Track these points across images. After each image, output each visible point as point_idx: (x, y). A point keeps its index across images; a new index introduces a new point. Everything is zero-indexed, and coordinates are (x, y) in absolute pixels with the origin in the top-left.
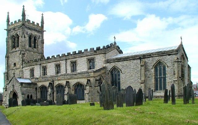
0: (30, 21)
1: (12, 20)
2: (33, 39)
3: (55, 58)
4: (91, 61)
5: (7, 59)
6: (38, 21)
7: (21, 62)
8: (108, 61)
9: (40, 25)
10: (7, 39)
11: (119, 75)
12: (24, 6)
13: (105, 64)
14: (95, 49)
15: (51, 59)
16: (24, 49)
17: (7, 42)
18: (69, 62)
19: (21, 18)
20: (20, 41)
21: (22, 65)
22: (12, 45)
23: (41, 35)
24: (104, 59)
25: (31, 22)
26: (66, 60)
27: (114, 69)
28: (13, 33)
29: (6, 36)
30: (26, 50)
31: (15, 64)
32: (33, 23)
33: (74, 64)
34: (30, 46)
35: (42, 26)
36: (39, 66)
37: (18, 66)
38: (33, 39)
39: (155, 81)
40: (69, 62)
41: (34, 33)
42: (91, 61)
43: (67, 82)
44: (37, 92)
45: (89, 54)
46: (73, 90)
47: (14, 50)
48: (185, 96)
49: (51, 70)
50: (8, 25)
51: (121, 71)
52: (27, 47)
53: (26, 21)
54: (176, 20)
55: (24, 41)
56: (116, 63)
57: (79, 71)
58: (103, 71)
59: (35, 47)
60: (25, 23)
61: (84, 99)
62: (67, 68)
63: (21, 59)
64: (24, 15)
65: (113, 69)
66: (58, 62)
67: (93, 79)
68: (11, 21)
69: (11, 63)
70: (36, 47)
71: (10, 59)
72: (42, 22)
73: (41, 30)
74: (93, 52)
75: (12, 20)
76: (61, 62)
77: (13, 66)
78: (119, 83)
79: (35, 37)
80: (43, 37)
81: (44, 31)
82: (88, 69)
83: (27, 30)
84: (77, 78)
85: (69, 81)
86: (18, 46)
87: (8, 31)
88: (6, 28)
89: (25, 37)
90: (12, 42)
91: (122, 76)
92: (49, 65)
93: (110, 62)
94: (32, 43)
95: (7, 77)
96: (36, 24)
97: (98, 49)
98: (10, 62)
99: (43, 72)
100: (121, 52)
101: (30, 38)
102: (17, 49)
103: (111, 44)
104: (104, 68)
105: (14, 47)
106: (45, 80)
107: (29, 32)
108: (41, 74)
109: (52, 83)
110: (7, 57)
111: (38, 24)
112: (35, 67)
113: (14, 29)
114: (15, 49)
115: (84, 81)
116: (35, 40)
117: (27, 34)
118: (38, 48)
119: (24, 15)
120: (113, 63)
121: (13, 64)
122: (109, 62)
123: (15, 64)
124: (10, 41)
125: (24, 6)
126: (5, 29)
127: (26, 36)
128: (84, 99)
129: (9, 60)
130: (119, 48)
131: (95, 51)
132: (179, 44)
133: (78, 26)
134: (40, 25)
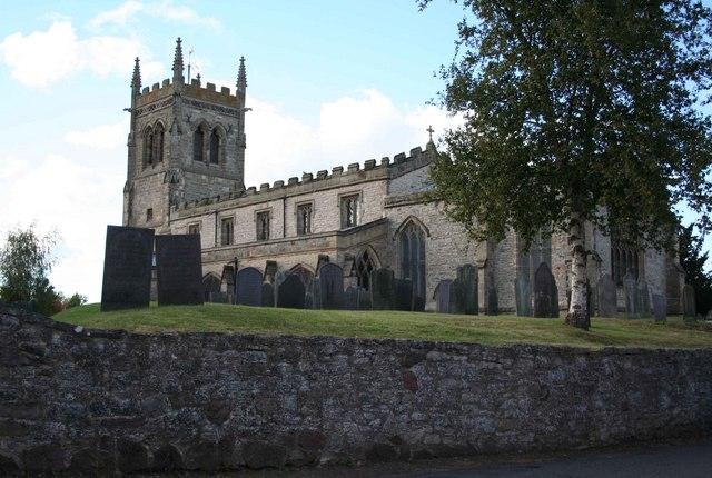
1: (147, 81)
2: (207, 136)
3: (256, 193)
4: (348, 203)
5: (127, 195)
6: (225, 80)
7: (166, 205)
8: (392, 204)
9: (233, 93)
10: (132, 138)
14: (362, 167)
15: (331, 177)
16: (177, 166)
17: (132, 145)
18: (292, 202)
19: (170, 75)
20: (166, 143)
21: (169, 214)
22: (145, 155)
23: (233, 121)
24: (384, 196)
26: (285, 198)
27: (409, 224)
28: (149, 119)
29: (127, 129)
30: (185, 170)
31: (150, 212)
33: (305, 211)
34: (199, 156)
35: (241, 94)
36: (213, 216)
38: (207, 136)
39: (519, 262)
41: (212, 117)
42: (348, 203)
43: (270, 264)
45: (344, 180)
47: (150, 169)
48: (611, 441)
49: (245, 231)
50: (136, 94)
51: (428, 231)
52: (189, 160)
55: (178, 145)
56: (416, 207)
58: (375, 233)
59: (215, 159)
60: (185, 92)
62: (288, 221)
63: (167, 197)
66: (264, 206)
67: (338, 256)
68: (144, 84)
69: (139, 209)
70: (220, 160)
71: (138, 197)
73: (232, 105)
74: (356, 176)
75: (147, 81)
76: (271, 204)
77: (144, 217)
79: (215, 131)
80: (241, 126)
81: (246, 110)
83: (186, 110)
84: (297, 253)
86: (161, 160)
87: (135, 113)
89: (180, 132)
90: (145, 146)
91: (430, 245)
92: (239, 213)
96: (218, 90)
97: (371, 165)
98: (136, 207)
99: (225, 234)
101: (199, 132)
102: (159, 167)
103: (416, 151)
104: (382, 222)
105: (150, 160)
106: (216, 257)
107: (197, 115)
108: (219, 241)
110: (130, 190)
111: (226, 90)
112: (204, 219)
114: (153, 167)
118: (224, 161)
120: (407, 208)
121: (145, 210)
123: (150, 212)
124: (140, 142)
127: (184, 126)
129: (135, 202)
131: (362, 174)
132: (428, 141)
133: (19, 34)
134: (233, 93)
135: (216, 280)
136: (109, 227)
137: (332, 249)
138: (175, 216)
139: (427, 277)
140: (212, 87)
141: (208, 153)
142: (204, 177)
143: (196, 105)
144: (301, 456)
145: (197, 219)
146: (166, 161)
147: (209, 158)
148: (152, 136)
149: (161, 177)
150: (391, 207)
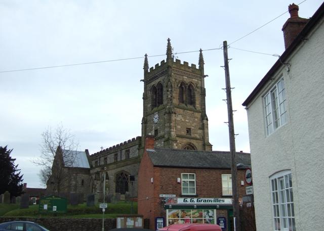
0: (179, 61)
1: (152, 64)
6: (193, 61)
9: (197, 67)
12: (169, 40)
19: (165, 58)
25: (182, 63)
32: (186, 63)
35: (201, 68)
44: (280, 224)
53: (175, 61)
57: (113, 154)
64: (169, 49)
72: (201, 61)
79: (189, 86)
81: (205, 76)
88: (143, 79)
95: (209, 168)
116: (190, 90)
119: (169, 49)
125: (169, 40)
126: (141, 80)
134: (197, 67)
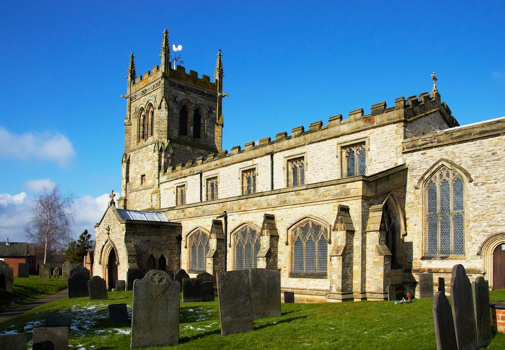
2: (191, 115)
11: (459, 192)
13: (405, 156)
18: (280, 159)
20: (156, 120)
23: (212, 135)
26: (272, 154)
37: (149, 181)
38: (191, 115)
40: (280, 159)
41: (196, 99)
46: (287, 244)
51: (467, 174)
54: (424, 151)
61: (323, 276)
65: (434, 173)
66: (250, 163)
71: (132, 166)
76: (256, 161)
78: (459, 220)
82: (286, 293)
85: (276, 213)
86: (152, 134)
93: (424, 149)
94: (188, 124)
100: (453, 123)
102: (150, 139)
106: (204, 212)
109: (222, 219)
113: (143, 92)
115: (326, 213)
117: (175, 101)
121: (139, 176)
122: (420, 150)
128: (326, 275)
130: (448, 111)
134: (213, 81)
135: (204, 235)
136: (412, 243)
137: (354, 197)
138: (163, 178)
139: (466, 230)
140: (194, 73)
141: (192, 128)
142: (188, 148)
143: (182, 88)
144: (187, 147)
145: (183, 180)
146: (156, 134)
147: (192, 134)
148: (144, 116)
149: (152, 147)
150: (414, 151)
